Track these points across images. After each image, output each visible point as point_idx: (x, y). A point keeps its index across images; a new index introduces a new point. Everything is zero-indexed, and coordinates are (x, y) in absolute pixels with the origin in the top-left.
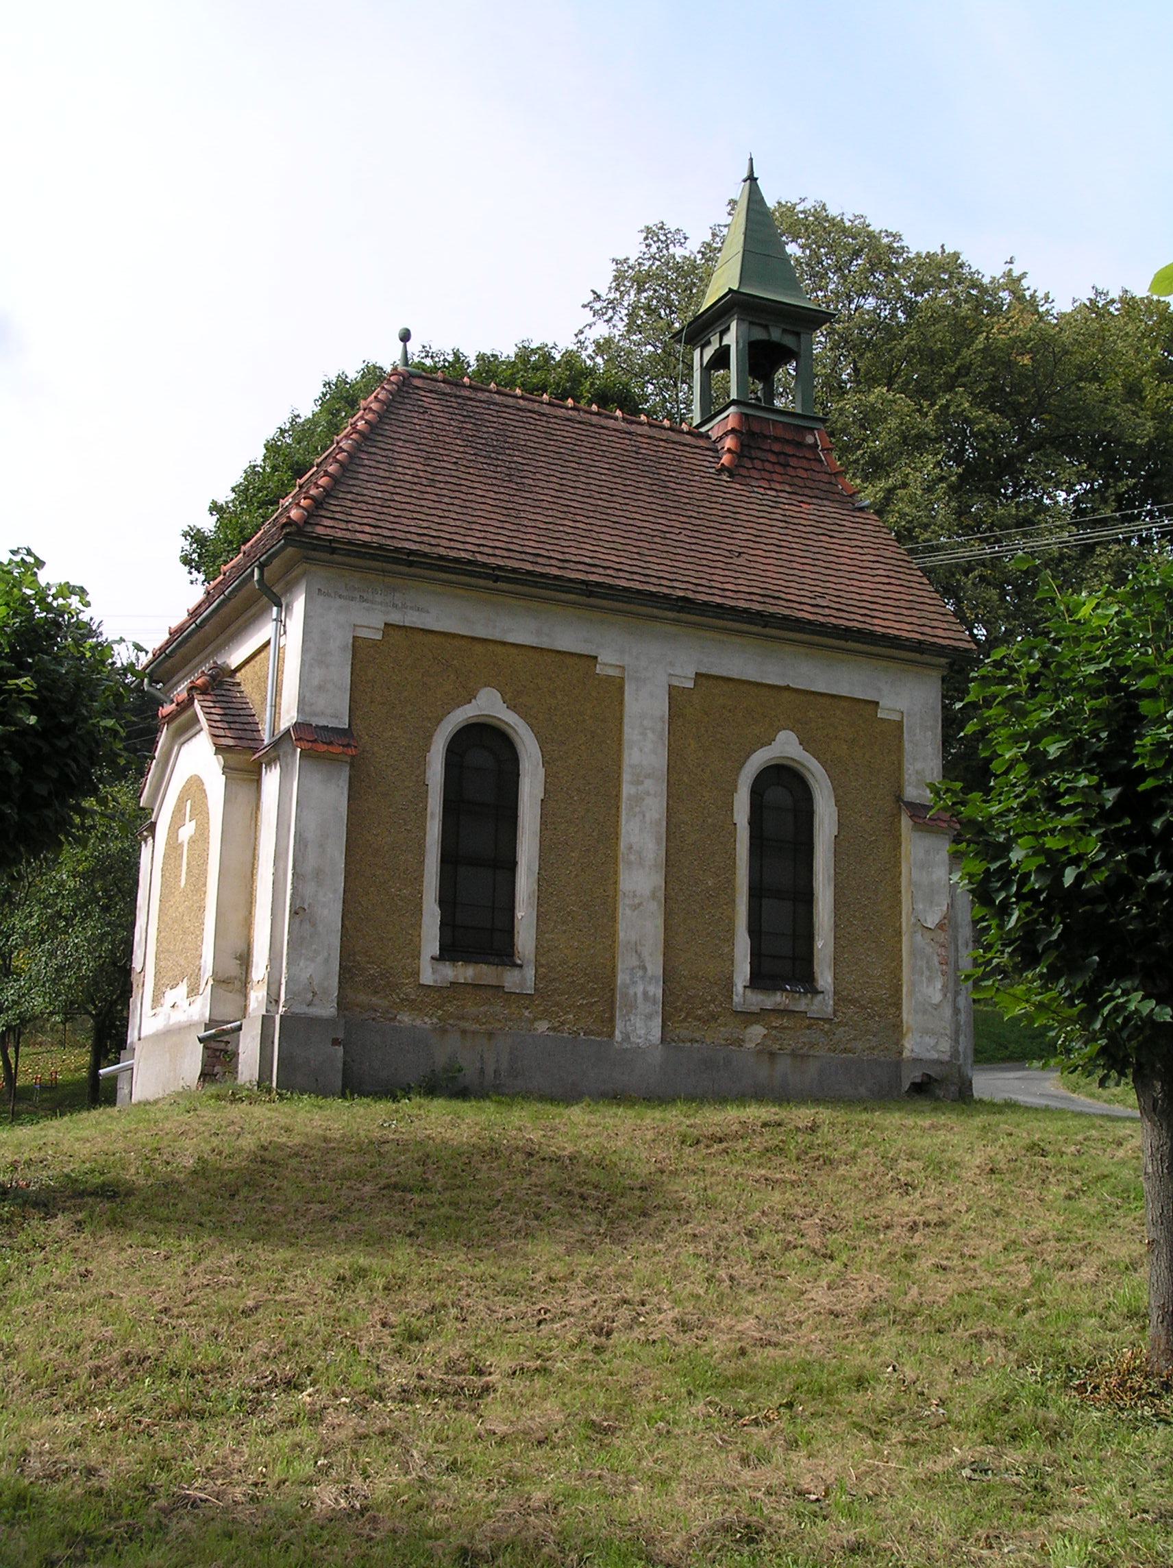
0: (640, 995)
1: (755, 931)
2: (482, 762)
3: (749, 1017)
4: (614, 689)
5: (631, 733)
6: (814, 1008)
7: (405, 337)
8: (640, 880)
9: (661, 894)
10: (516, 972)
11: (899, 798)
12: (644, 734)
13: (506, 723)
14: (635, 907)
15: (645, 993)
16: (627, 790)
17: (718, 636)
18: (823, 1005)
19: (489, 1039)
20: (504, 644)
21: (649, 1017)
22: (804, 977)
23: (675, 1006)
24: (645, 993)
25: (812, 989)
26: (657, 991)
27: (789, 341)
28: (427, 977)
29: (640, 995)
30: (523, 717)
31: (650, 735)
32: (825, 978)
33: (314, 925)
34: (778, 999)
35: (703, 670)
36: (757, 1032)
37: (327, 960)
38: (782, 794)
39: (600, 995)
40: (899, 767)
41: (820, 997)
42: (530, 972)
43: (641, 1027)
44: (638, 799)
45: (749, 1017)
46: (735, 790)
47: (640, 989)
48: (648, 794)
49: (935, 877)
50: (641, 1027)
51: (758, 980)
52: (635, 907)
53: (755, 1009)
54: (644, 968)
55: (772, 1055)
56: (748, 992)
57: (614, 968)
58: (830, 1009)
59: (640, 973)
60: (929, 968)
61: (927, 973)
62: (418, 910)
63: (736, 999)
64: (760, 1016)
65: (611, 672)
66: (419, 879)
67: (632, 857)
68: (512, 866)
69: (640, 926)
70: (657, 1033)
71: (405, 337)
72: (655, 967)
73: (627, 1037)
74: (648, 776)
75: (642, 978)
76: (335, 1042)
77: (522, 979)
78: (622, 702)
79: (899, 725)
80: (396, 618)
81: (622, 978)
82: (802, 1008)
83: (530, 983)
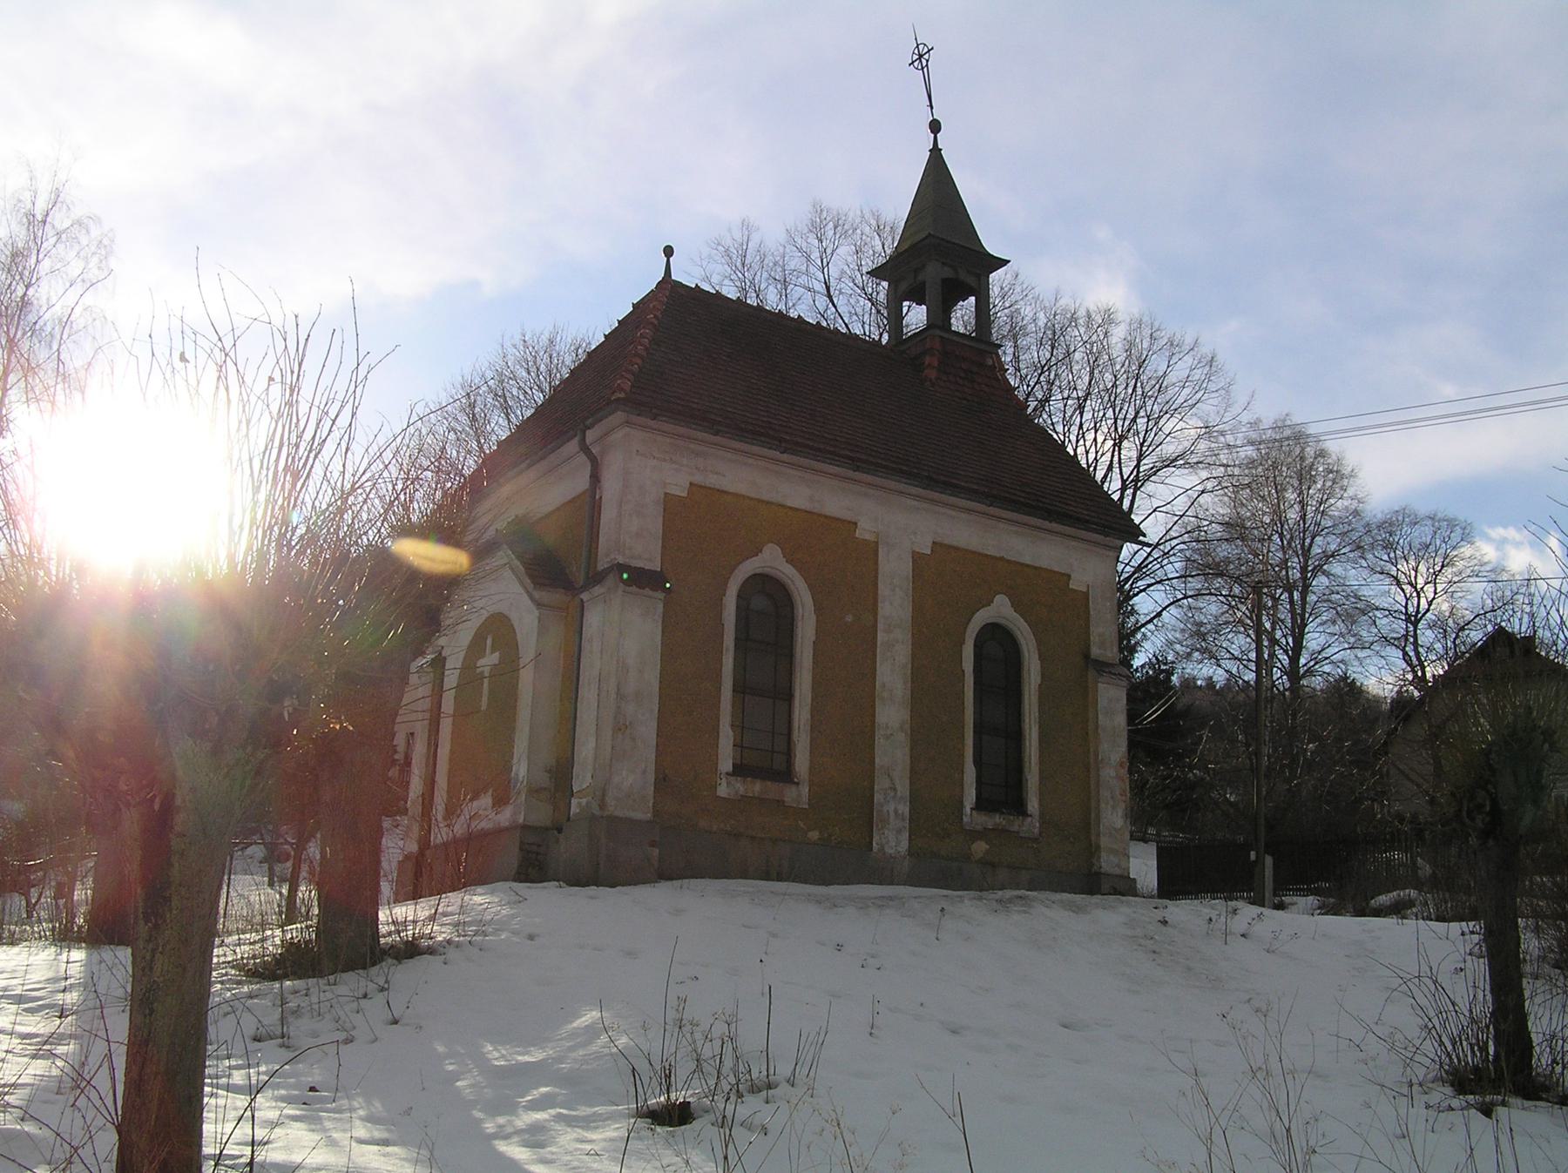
1: (978, 762)
2: (767, 611)
4: (870, 551)
5: (883, 589)
7: (669, 251)
8: (892, 715)
9: (907, 726)
10: (794, 788)
11: (1087, 656)
13: (522, 583)
14: (887, 737)
15: (896, 811)
16: (881, 637)
18: (1031, 825)
19: (1463, 1081)
20: (783, 506)
21: (899, 831)
22: (1018, 806)
23: (921, 821)
24: (896, 811)
26: (905, 809)
27: (971, 281)
28: (723, 790)
30: (799, 570)
32: (1033, 805)
33: (634, 739)
34: (997, 819)
35: (939, 540)
36: (980, 847)
37: (644, 772)
38: (998, 650)
39: (866, 817)
40: (1088, 633)
42: (805, 790)
43: (893, 840)
46: (963, 642)
47: (891, 807)
50: (893, 840)
51: (982, 805)
52: (887, 737)
53: (979, 828)
55: (993, 865)
57: (873, 788)
62: (715, 731)
65: (867, 537)
66: (716, 706)
67: (885, 695)
68: (789, 697)
69: (892, 753)
70: (904, 845)
71: (669, 251)
72: (903, 788)
73: (882, 849)
76: (653, 844)
77: (798, 795)
78: (876, 563)
79: (1086, 595)
81: (878, 797)
82: (1016, 828)
83: (805, 799)
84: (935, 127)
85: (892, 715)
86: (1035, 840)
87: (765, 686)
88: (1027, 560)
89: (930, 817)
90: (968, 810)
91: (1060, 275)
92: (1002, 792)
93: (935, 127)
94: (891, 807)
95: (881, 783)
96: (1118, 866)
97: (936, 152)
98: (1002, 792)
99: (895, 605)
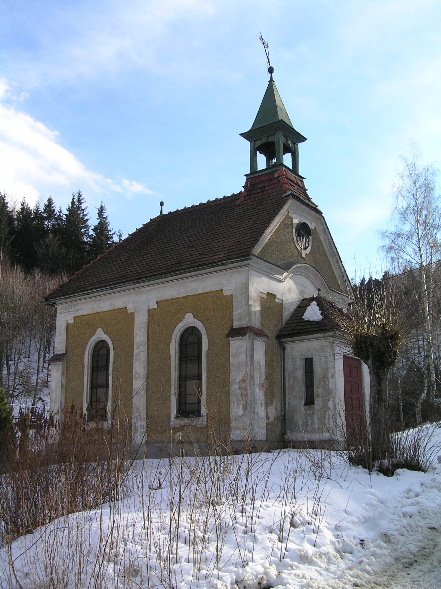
0: (139, 426)
3: (176, 430)
5: (136, 331)
6: (199, 423)
7: (162, 204)
8: (139, 383)
9: (145, 388)
12: (140, 330)
15: (141, 425)
16: (135, 352)
17: (199, 277)
23: (150, 428)
25: (199, 415)
26: (144, 423)
29: (139, 426)
31: (142, 329)
32: (203, 411)
36: (179, 436)
41: (202, 418)
43: (139, 437)
44: (138, 354)
45: (176, 430)
47: (139, 424)
48: (141, 351)
49: (240, 359)
54: (140, 416)
56: (175, 419)
58: (205, 423)
59: (139, 418)
60: (237, 400)
61: (237, 402)
63: (171, 423)
64: (181, 428)
67: (137, 376)
71: (162, 204)
74: (141, 345)
75: (140, 419)
80: (76, 314)
82: (195, 424)
84: (271, 70)
85: (139, 383)
86: (205, 427)
87: (98, 385)
88: (200, 291)
89: (155, 424)
90: (172, 418)
91: (247, 127)
92: (187, 409)
93: (271, 70)
94: (139, 424)
95: (135, 414)
96: (240, 435)
97: (271, 81)
98: (187, 409)
99: (140, 336)
